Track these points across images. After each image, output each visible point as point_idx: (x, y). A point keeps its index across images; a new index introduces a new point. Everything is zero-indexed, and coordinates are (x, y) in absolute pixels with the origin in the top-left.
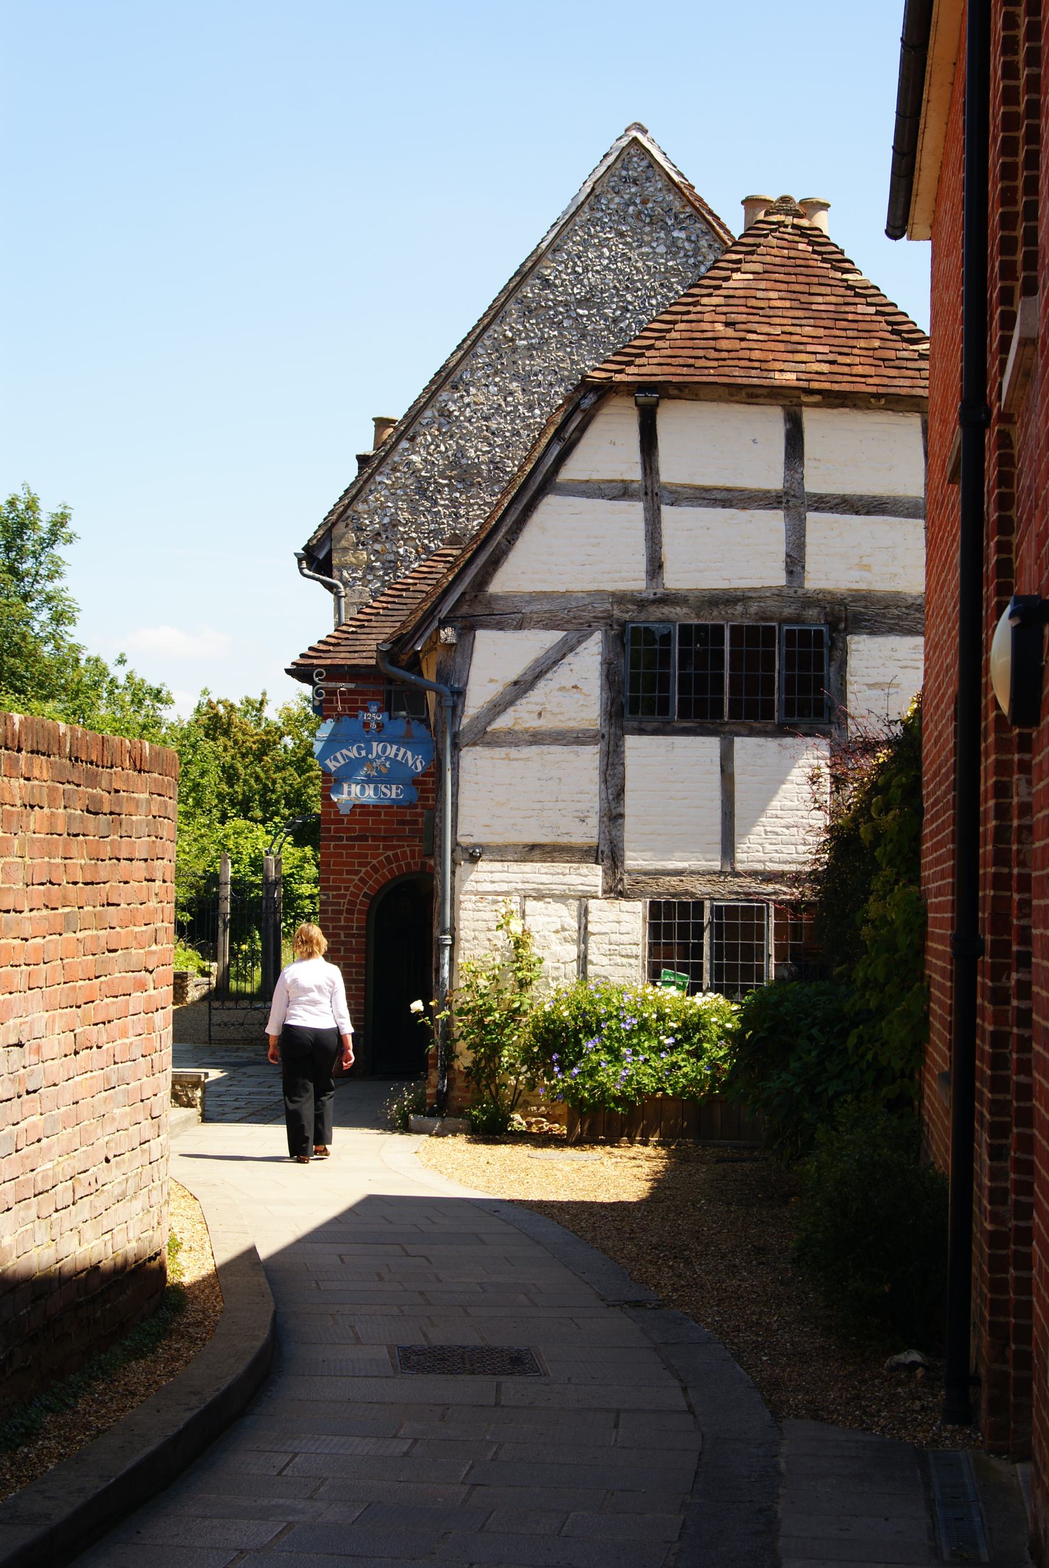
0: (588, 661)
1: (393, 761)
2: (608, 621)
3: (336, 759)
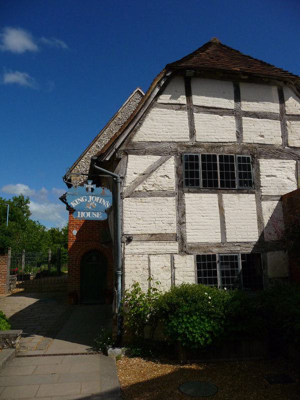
0: (170, 166)
1: (98, 203)
2: (175, 152)
3: (75, 202)
